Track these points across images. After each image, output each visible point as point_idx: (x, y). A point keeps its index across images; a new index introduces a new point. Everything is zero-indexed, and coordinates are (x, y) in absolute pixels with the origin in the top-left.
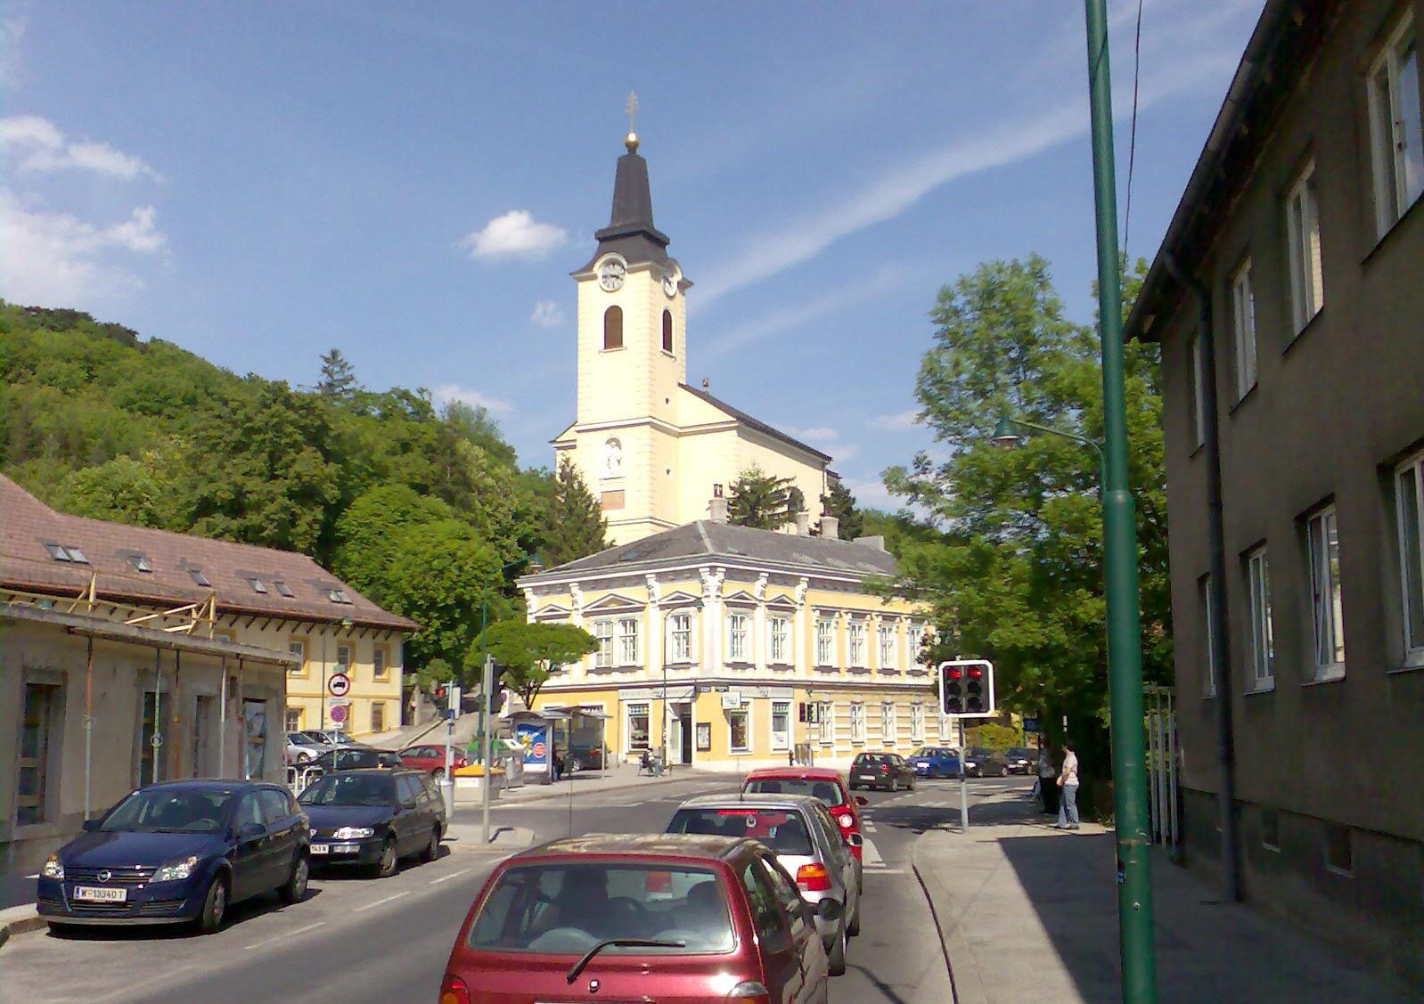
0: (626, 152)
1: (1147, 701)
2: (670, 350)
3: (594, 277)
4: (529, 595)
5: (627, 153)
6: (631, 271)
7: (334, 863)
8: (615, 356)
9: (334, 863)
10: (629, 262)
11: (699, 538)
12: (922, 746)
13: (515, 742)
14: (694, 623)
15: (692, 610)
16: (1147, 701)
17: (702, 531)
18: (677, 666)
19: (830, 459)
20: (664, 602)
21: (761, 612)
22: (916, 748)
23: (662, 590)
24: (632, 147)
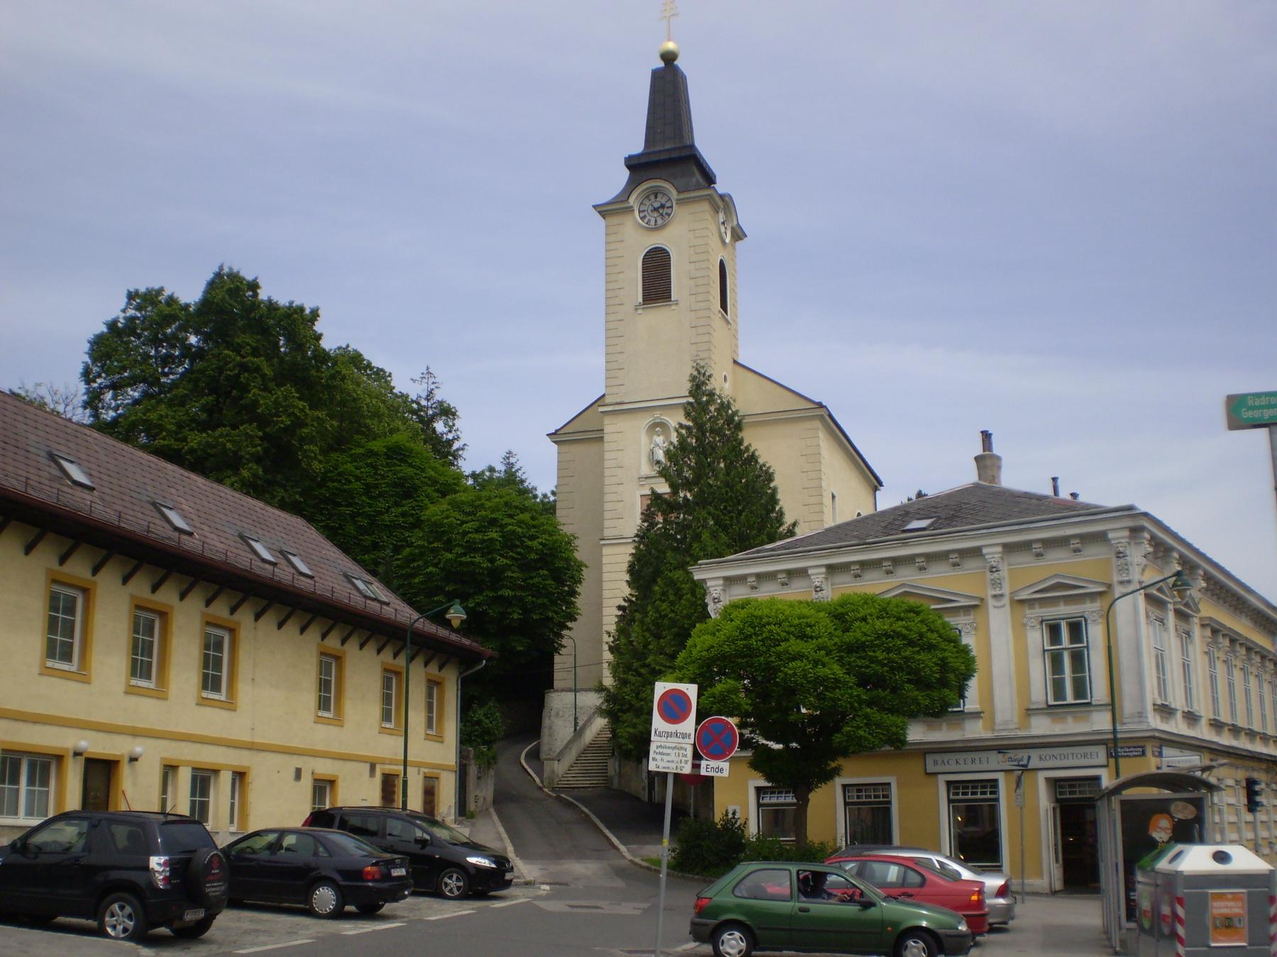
0: (661, 64)
8: (659, 316)
10: (679, 192)
20: (1024, 595)
24: (669, 58)
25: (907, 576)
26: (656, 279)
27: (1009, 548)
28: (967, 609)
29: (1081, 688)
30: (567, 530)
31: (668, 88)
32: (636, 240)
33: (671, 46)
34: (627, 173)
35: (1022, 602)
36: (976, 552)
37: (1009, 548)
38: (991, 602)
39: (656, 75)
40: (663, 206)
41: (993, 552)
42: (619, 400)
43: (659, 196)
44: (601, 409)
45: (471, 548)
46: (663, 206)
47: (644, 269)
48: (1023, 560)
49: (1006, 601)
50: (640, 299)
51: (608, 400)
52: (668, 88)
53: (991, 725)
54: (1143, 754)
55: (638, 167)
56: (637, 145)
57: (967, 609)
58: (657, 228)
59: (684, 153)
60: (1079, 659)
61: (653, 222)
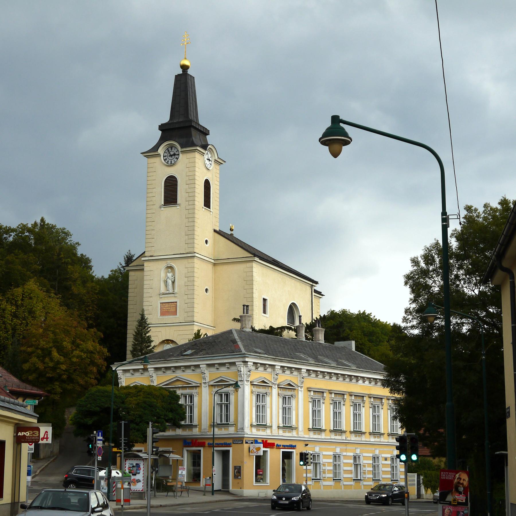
0: (180, 71)
1: (151, 491)
2: (209, 207)
3: (159, 155)
4: (120, 373)
5: (182, 73)
6: (183, 152)
7: (498, 453)
8: (171, 210)
9: (498, 453)
10: (182, 147)
11: (234, 342)
12: (380, 483)
13: (118, 471)
14: (232, 398)
15: (231, 389)
16: (151, 491)
17: (236, 337)
18: (220, 425)
19: (316, 283)
20: (212, 383)
21: (275, 391)
22: (376, 484)
23: (211, 375)
24: (185, 68)
25: (179, 374)
26: (171, 192)
27: (209, 365)
28: (196, 387)
29: (227, 419)
30: (356, 312)
31: (184, 85)
32: (161, 171)
33: (187, 63)
34: (160, 132)
35: (212, 385)
36: (198, 366)
37: (209, 365)
38: (203, 385)
39: (177, 77)
40: (174, 155)
41: (203, 367)
42: (152, 254)
43: (173, 148)
44: (143, 259)
45: (493, 254)
46: (174, 155)
47: (165, 186)
48: (213, 369)
49: (207, 385)
50: (163, 203)
51: (146, 254)
52: (184, 85)
53: (200, 429)
54: (242, 443)
55: (168, 131)
56: (166, 119)
57: (196, 387)
58: (172, 165)
59: (187, 124)
60: (227, 407)
61: (169, 163)
